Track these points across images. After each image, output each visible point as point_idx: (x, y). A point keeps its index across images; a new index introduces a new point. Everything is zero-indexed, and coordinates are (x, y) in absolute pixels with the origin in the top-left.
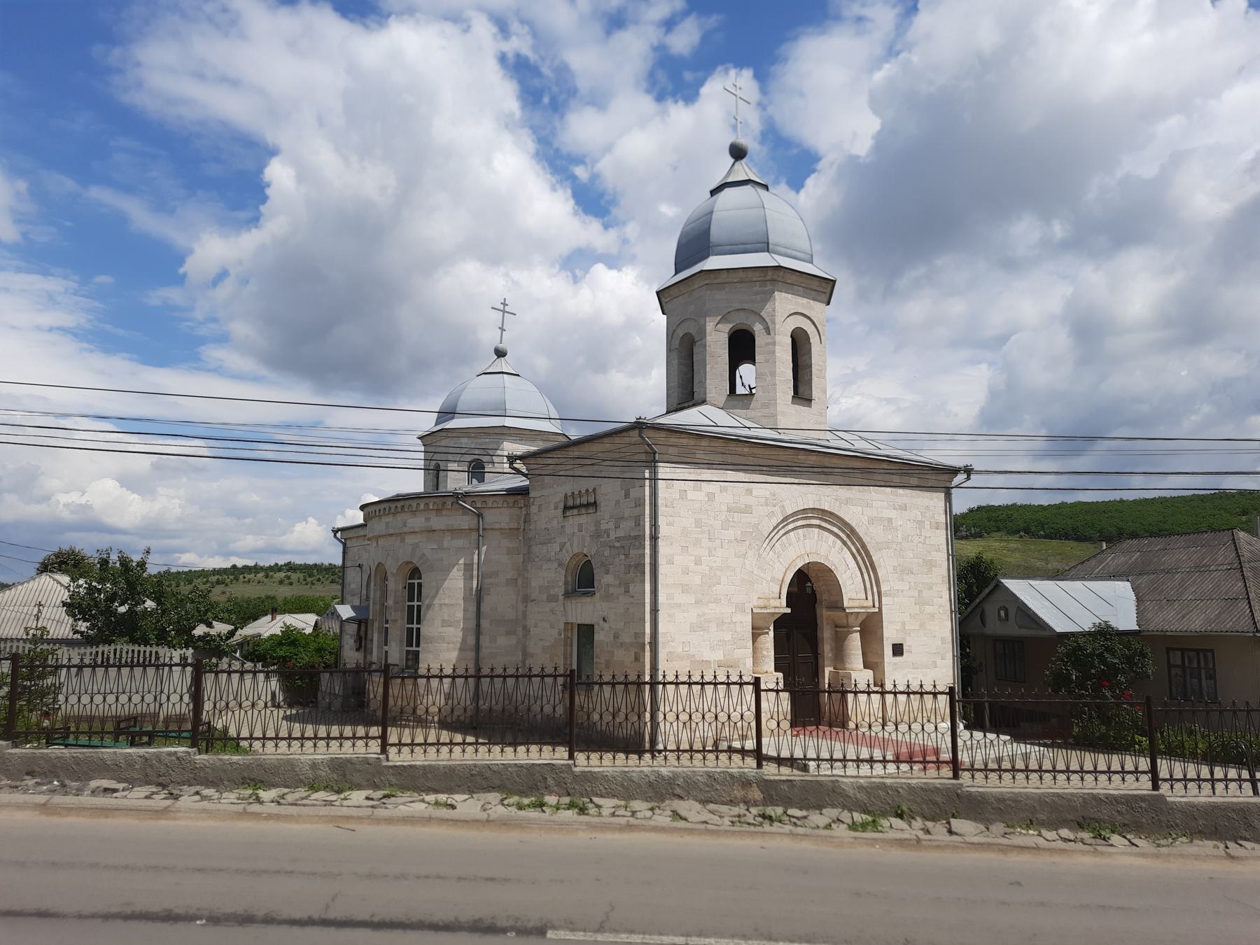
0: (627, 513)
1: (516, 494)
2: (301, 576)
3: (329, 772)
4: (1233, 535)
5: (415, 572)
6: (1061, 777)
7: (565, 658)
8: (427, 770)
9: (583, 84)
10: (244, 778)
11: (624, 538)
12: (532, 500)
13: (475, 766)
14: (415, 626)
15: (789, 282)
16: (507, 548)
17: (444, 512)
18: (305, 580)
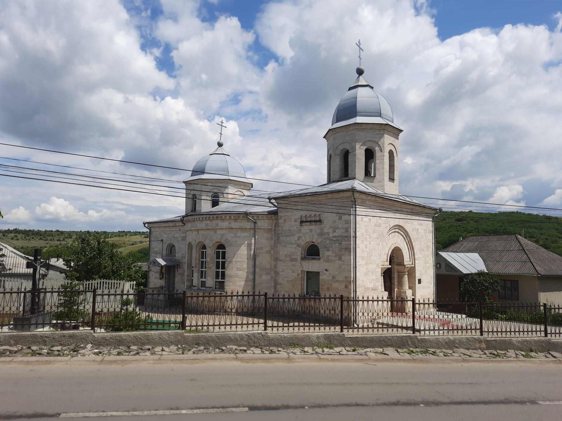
0: (340, 226)
1: (271, 214)
2: (23, 236)
3: (324, 340)
4: (516, 236)
5: (221, 246)
6: (366, 330)
7: (301, 286)
8: (363, 339)
9: (165, 9)
10: (290, 343)
11: (339, 236)
12: (280, 217)
13: (381, 337)
14: (204, 270)
15: (389, 130)
16: (266, 237)
17: (238, 221)
18: (25, 238)
